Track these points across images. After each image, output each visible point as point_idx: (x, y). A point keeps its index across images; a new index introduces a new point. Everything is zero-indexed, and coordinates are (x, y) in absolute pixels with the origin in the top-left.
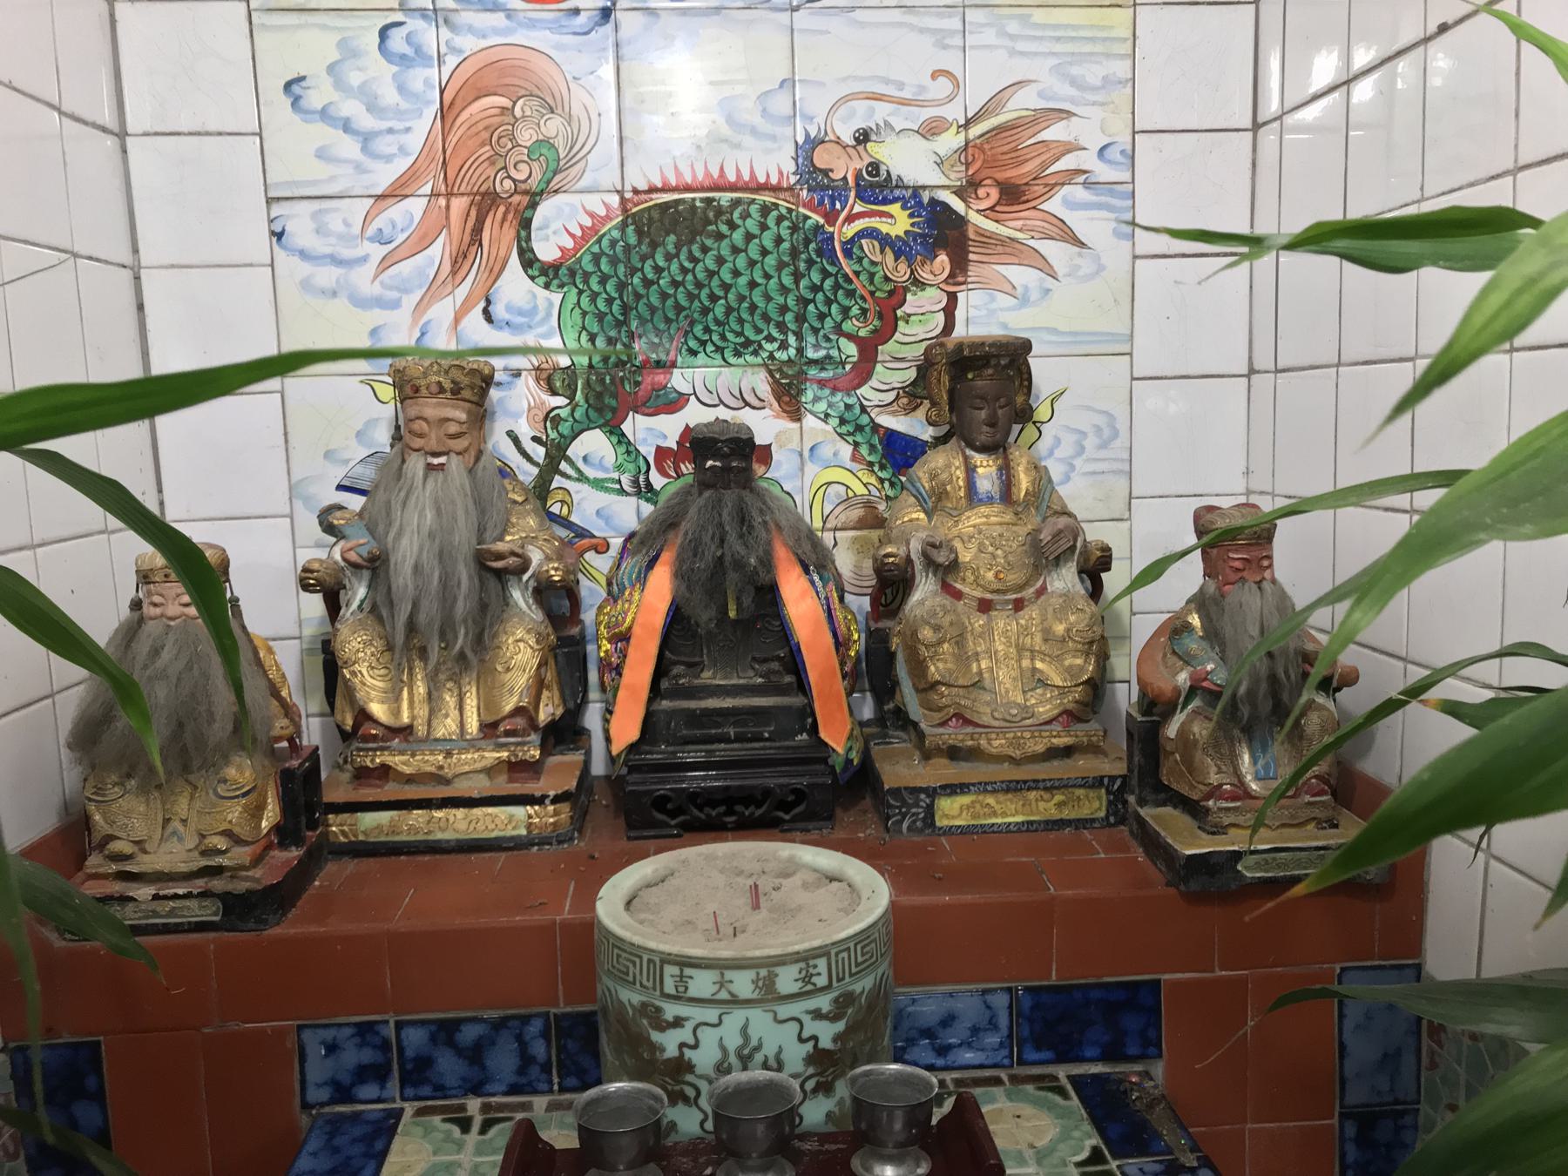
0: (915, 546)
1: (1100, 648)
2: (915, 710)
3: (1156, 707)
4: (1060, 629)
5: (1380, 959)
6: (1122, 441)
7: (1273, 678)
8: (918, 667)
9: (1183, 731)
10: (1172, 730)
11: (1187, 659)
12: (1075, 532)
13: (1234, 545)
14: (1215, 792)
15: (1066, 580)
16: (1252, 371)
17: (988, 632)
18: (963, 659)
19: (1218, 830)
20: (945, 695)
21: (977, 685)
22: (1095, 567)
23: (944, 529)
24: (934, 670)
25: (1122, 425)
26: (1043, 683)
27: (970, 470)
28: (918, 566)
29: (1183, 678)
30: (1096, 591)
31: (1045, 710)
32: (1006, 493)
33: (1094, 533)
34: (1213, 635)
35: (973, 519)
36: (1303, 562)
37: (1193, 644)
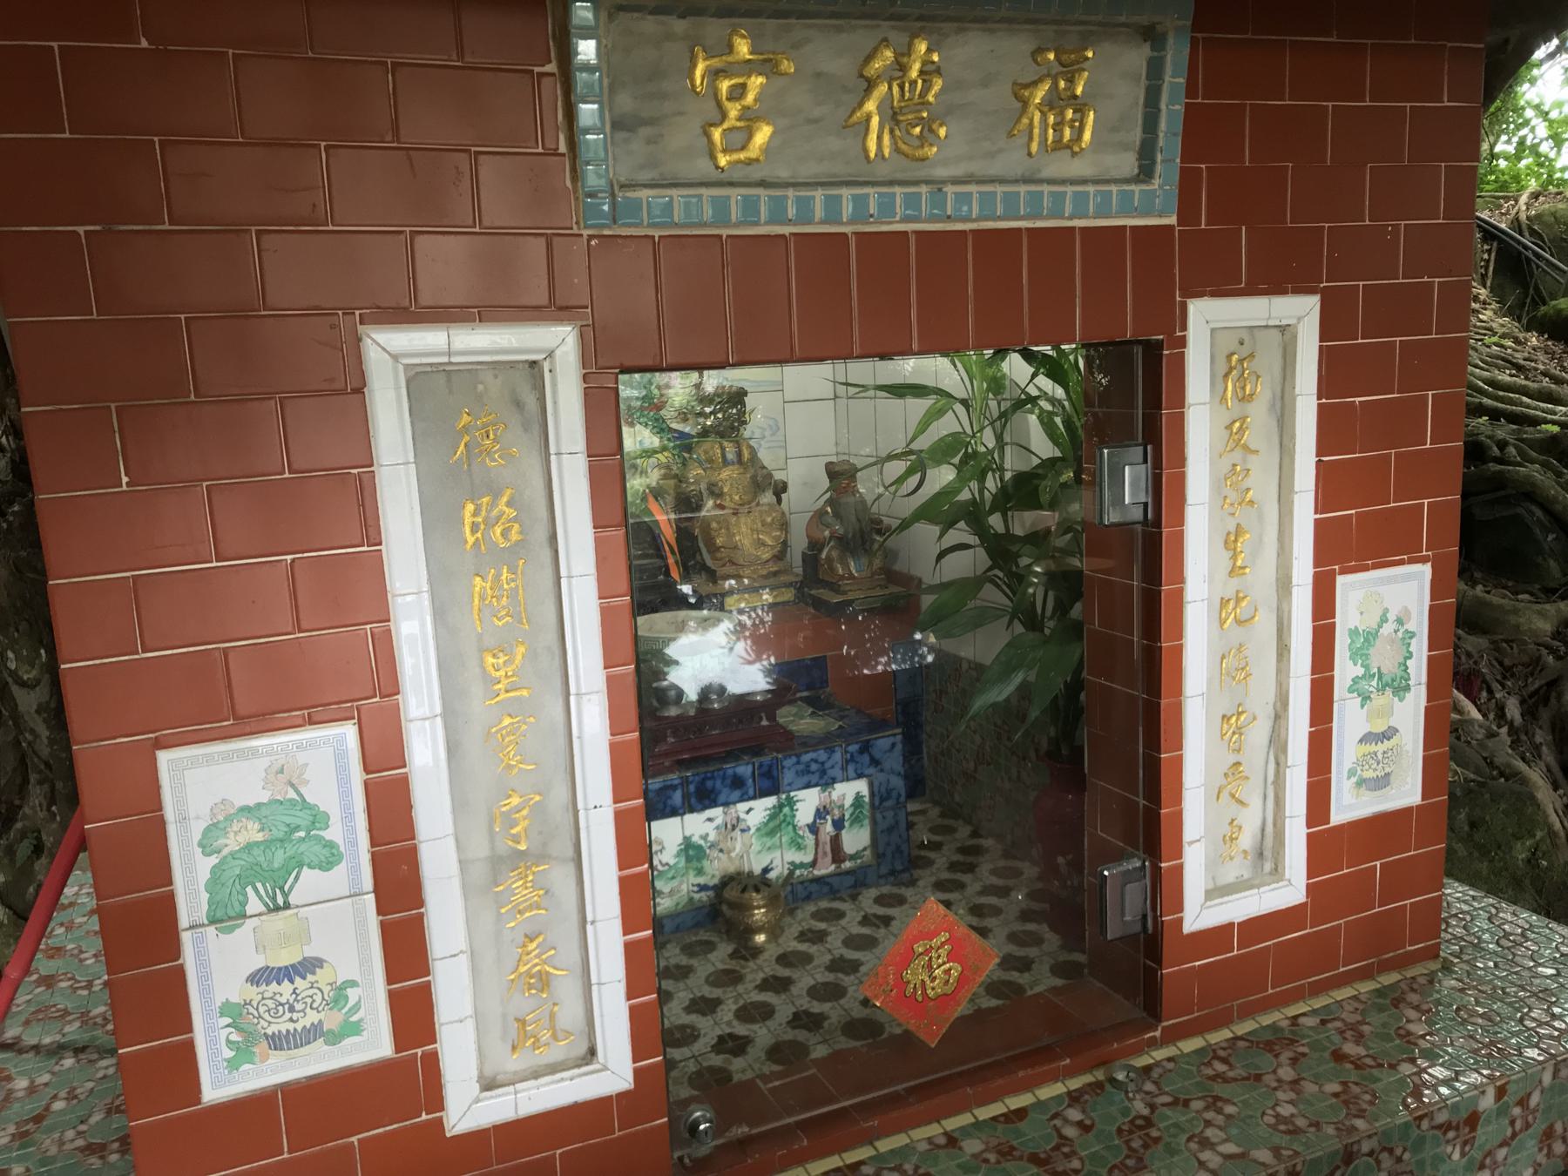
0: (703, 486)
1: (784, 526)
2: (709, 562)
3: (815, 546)
4: (769, 520)
5: (1133, 406)
6: (781, 432)
7: (861, 530)
8: (710, 543)
9: (828, 556)
10: (824, 556)
11: (828, 526)
12: (770, 476)
13: (840, 476)
14: (842, 578)
15: (768, 498)
16: (836, 397)
17: (738, 524)
18: (730, 535)
19: (845, 593)
20: (723, 553)
21: (736, 547)
22: (780, 489)
23: (715, 477)
24: (719, 541)
25: (781, 425)
26: (764, 544)
27: (723, 449)
28: (705, 494)
29: (827, 533)
30: (779, 501)
31: (766, 556)
32: (740, 461)
33: (778, 476)
34: (836, 514)
35: (725, 474)
36: (867, 486)
37: (830, 519)
